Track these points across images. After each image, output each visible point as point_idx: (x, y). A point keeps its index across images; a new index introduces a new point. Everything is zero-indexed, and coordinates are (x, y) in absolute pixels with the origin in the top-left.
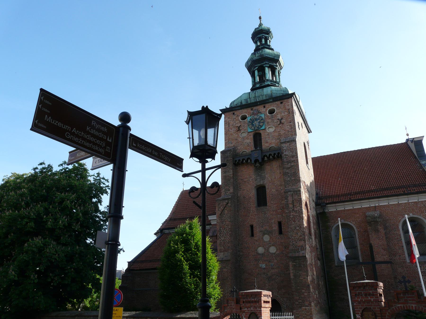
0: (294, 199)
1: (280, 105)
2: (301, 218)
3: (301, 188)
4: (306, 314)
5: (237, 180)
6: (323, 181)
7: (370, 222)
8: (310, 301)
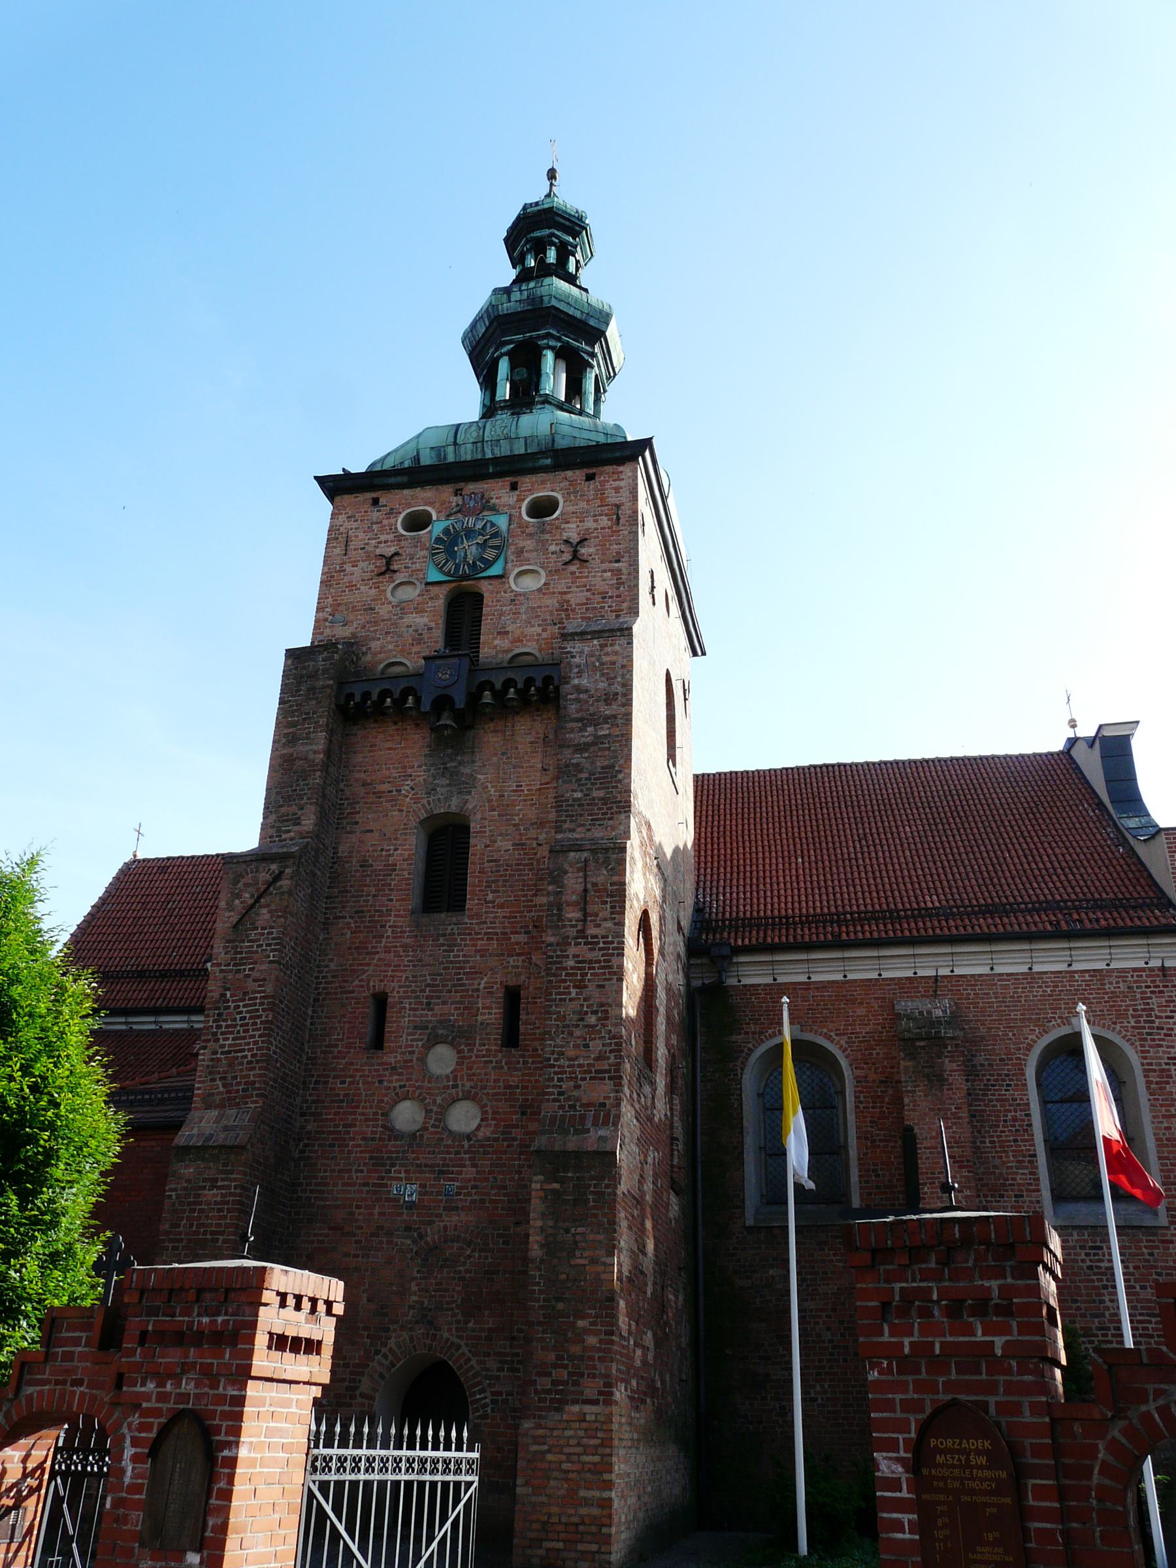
0: (589, 886)
1: (585, 486)
2: (615, 973)
3: (627, 836)
4: (585, 1441)
5: (342, 786)
6: (729, 863)
7: (909, 1039)
8: (608, 1376)
